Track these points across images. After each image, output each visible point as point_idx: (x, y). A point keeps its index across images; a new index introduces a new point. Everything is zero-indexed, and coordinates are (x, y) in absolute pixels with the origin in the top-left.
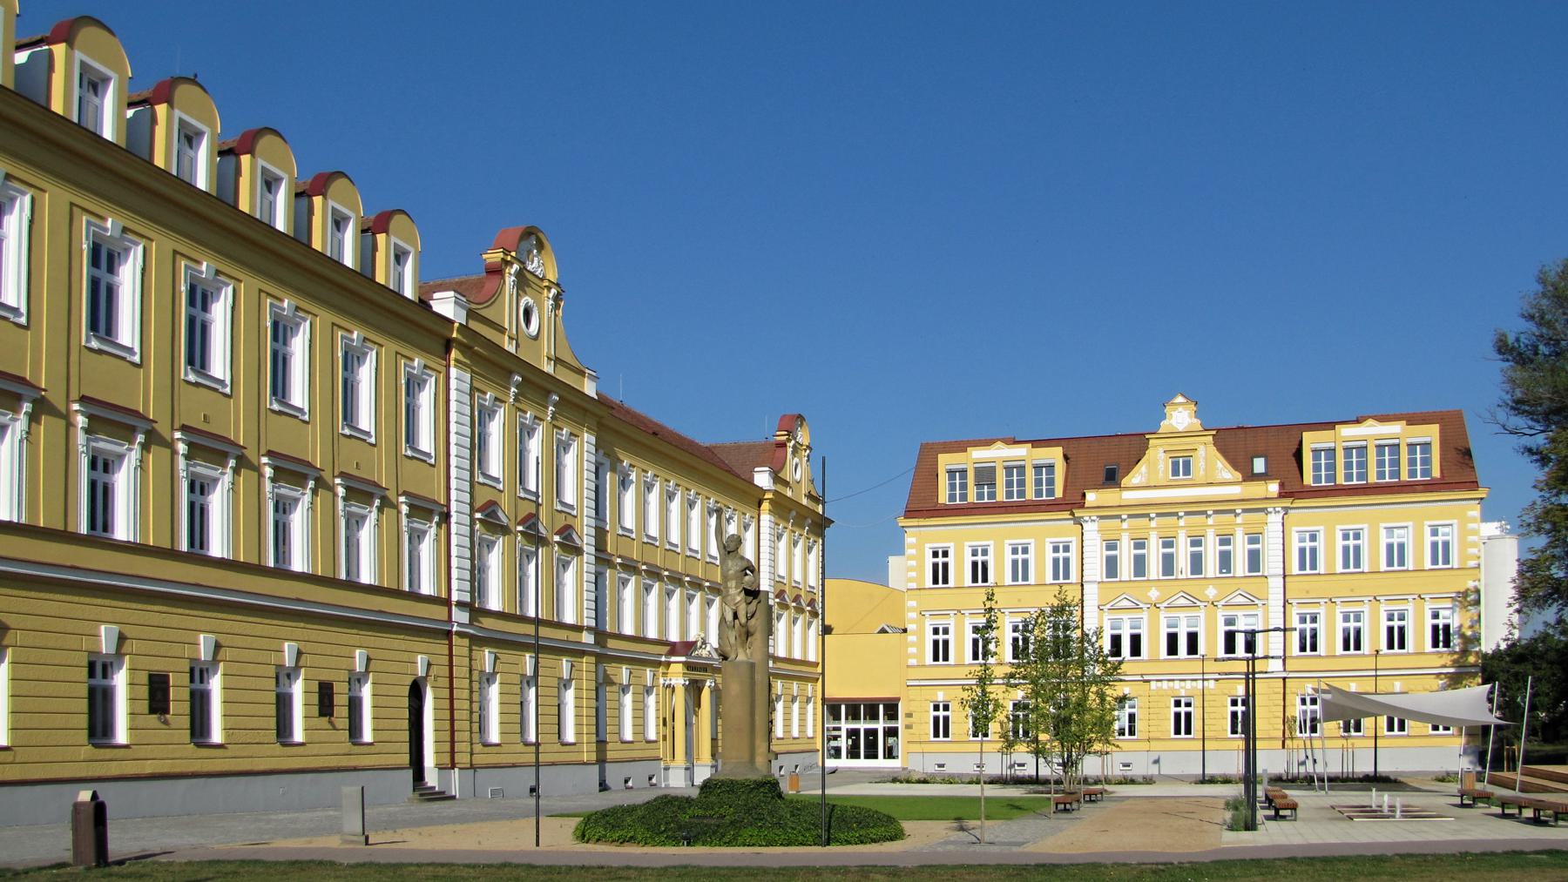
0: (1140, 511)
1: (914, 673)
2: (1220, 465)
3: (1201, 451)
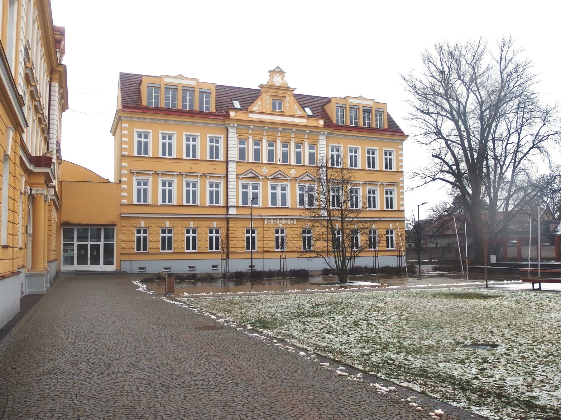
1: (124, 210)
2: (296, 107)
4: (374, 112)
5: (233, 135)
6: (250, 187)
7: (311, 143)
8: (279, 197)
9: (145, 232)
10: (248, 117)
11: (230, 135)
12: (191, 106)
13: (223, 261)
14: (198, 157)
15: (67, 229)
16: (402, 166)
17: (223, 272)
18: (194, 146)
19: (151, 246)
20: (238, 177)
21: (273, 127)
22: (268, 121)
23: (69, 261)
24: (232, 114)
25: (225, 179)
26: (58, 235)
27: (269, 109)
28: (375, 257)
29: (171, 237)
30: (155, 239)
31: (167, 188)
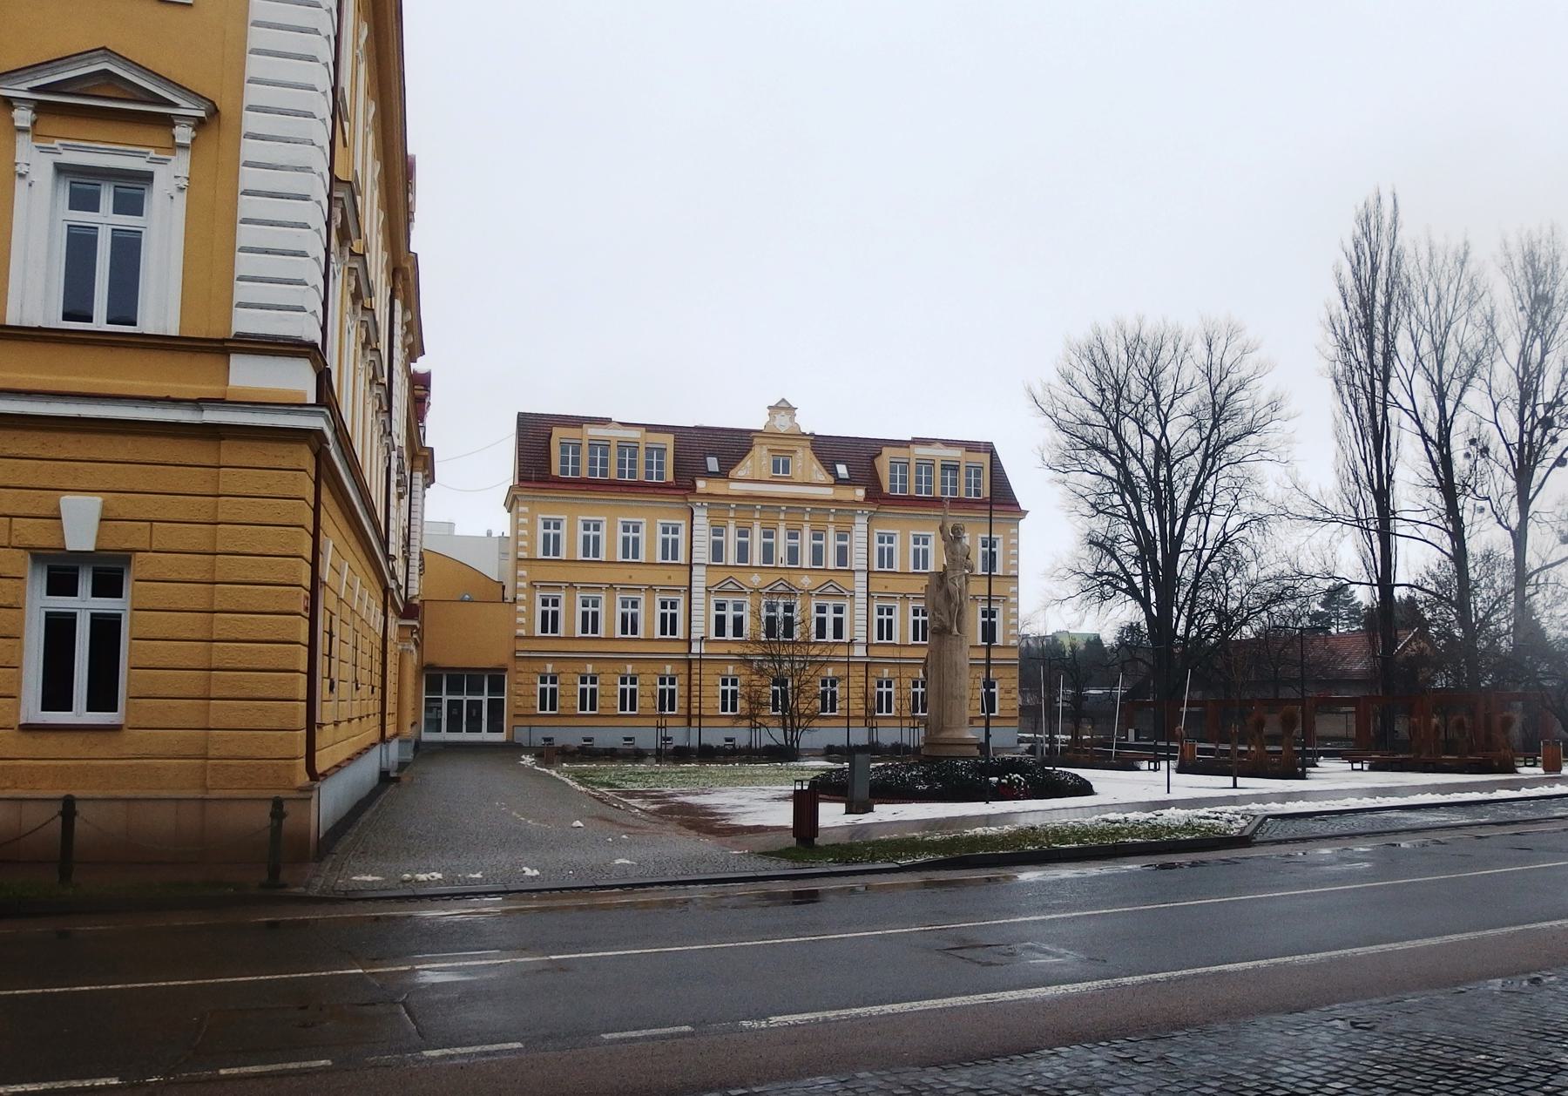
1: (521, 645)
3: (800, 454)
4: (963, 470)
8: (729, 623)
12: (903, 489)
15: (432, 676)
16: (1016, 566)
20: (708, 591)
23: (434, 725)
24: (701, 485)
26: (417, 684)
27: (767, 473)
31: (669, 611)
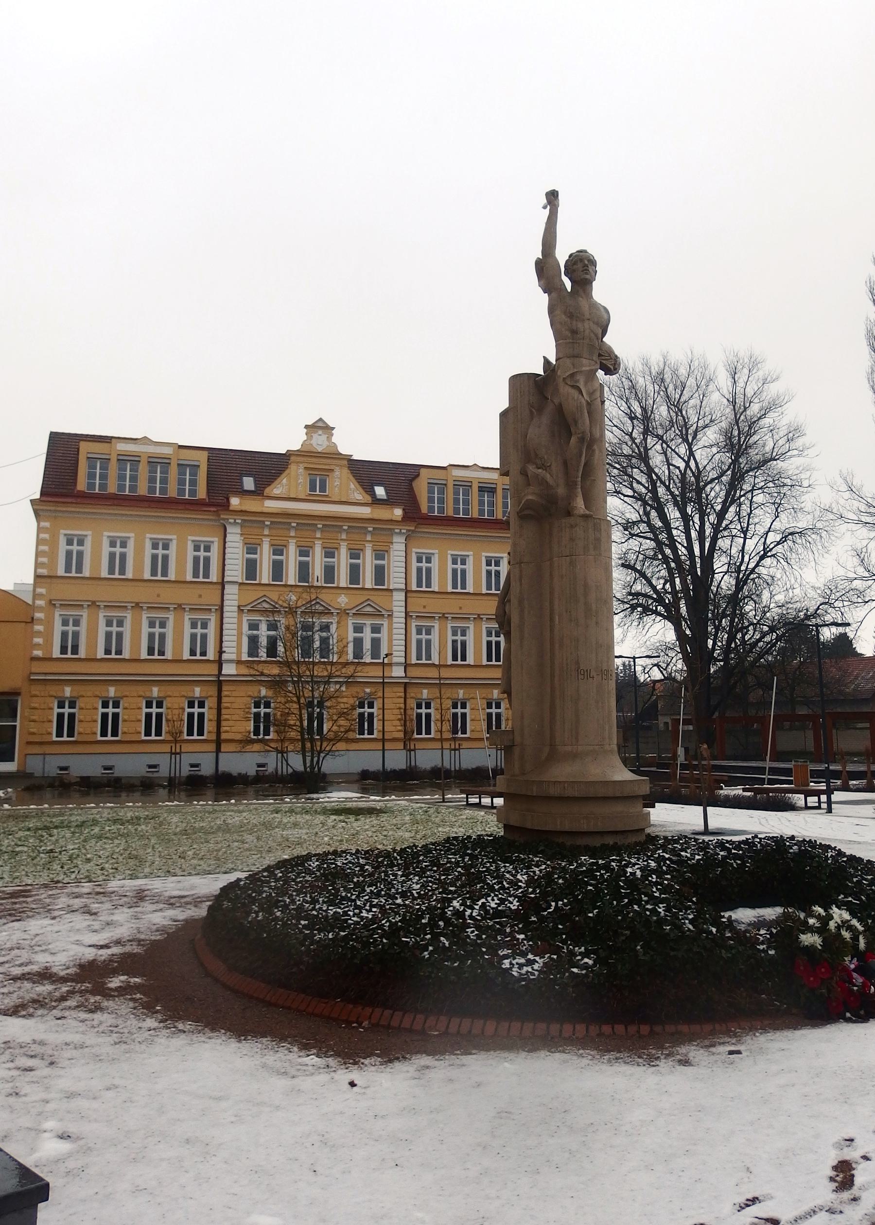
0: (282, 519)
1: (36, 667)
2: (352, 486)
5: (235, 537)
6: (367, 630)
7: (303, 544)
9: (116, 705)
10: (263, 506)
11: (229, 538)
13: (173, 756)
14: (470, 589)
17: (172, 775)
18: (464, 572)
19: (81, 730)
20: (240, 610)
21: (307, 522)
22: (290, 512)
25: (219, 613)
27: (303, 490)
28: (455, 750)
29: (465, 714)
30: (88, 718)
